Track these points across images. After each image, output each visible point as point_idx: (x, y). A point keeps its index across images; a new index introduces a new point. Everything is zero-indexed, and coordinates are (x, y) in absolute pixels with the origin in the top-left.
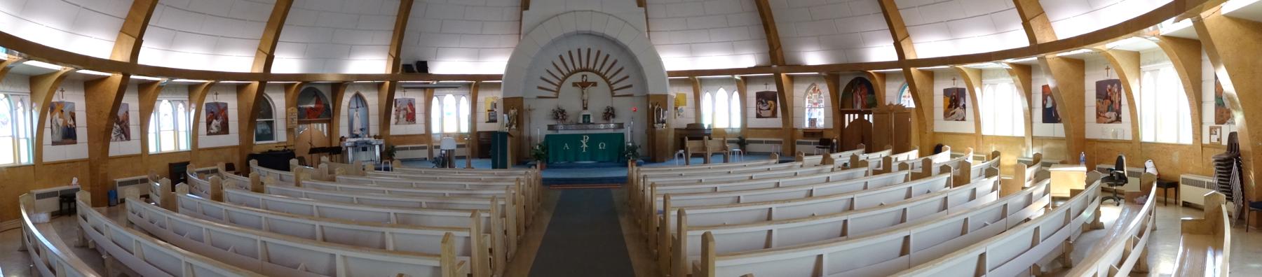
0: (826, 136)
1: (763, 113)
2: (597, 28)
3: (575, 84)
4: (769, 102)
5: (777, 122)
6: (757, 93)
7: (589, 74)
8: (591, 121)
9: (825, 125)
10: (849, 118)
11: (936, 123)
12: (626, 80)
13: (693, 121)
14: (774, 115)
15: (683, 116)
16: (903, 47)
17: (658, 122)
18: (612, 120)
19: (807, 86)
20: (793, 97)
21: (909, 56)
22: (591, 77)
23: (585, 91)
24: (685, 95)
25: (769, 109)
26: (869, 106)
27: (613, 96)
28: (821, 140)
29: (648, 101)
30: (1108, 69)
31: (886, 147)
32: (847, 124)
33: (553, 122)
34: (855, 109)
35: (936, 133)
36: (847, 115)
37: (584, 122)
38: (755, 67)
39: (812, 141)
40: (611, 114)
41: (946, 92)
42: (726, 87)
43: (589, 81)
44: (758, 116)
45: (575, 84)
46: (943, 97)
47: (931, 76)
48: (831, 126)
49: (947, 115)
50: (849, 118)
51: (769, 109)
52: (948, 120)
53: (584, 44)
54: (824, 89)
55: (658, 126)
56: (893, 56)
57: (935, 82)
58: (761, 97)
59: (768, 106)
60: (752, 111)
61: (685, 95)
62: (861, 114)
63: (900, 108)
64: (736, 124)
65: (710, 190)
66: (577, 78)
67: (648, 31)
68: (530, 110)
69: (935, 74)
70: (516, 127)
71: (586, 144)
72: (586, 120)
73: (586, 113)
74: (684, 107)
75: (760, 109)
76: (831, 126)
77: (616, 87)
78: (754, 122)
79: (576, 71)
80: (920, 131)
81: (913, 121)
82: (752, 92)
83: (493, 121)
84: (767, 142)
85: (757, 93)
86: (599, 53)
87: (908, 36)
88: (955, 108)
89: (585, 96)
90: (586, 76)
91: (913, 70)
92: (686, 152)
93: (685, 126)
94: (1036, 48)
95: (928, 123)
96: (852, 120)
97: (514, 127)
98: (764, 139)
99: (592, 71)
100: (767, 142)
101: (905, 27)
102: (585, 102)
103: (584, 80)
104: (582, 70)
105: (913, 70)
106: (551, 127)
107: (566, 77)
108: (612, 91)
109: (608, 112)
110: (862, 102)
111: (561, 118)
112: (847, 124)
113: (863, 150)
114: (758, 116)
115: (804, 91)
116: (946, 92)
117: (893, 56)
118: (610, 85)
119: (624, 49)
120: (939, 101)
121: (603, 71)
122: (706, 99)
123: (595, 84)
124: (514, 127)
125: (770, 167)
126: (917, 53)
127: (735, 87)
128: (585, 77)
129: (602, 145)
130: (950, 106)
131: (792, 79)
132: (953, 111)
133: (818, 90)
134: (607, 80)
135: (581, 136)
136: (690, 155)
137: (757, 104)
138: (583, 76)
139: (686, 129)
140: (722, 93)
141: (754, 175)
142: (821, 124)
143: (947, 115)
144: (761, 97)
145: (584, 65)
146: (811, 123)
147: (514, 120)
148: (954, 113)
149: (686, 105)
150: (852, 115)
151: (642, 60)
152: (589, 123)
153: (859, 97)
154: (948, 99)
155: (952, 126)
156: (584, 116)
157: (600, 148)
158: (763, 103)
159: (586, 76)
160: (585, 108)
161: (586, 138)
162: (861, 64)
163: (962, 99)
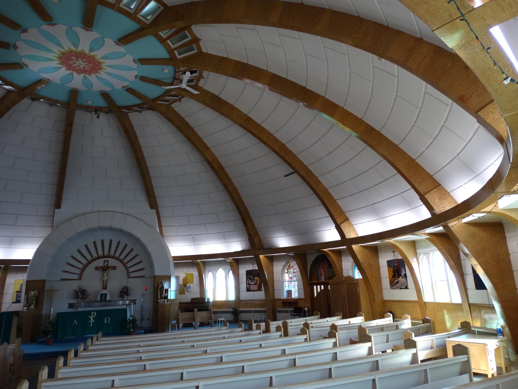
0: (300, 305)
1: (252, 287)
2: (116, 225)
3: (97, 268)
4: (256, 278)
5: (260, 295)
6: (247, 271)
7: (109, 259)
8: (108, 299)
9: (298, 296)
10: (317, 289)
11: (384, 291)
12: (140, 264)
13: (198, 296)
14: (259, 289)
15: (190, 292)
16: (343, 229)
17: (161, 298)
18: (126, 298)
19: (283, 263)
20: (273, 273)
21: (350, 235)
22: (112, 262)
23: (105, 274)
24: (193, 274)
25: (256, 284)
26: (330, 278)
27: (129, 277)
28: (295, 309)
29: (154, 281)
30: (394, 252)
31: (336, 314)
32: (315, 294)
33: (73, 301)
34: (320, 281)
35: (385, 301)
36: (315, 287)
37: (101, 300)
38: (241, 251)
39: (289, 309)
40: (125, 292)
41: (389, 263)
42: (224, 267)
43: (110, 265)
44: (248, 290)
45: (97, 268)
46: (387, 268)
47: (375, 250)
48: (303, 297)
49: (393, 284)
50: (317, 289)
51: (256, 284)
52: (394, 289)
53: (107, 237)
54: (295, 267)
55: (160, 301)
56: (337, 237)
57: (380, 255)
58: (249, 273)
59: (255, 282)
60: (243, 286)
61: (193, 274)
62: (326, 285)
63: (351, 279)
64: (232, 297)
65: (213, 361)
66: (100, 263)
67: (160, 226)
68: (52, 291)
69: (379, 249)
70: (35, 306)
71: (93, 319)
72: (103, 298)
73: (104, 292)
74: (192, 285)
75: (249, 284)
76: (303, 297)
77: (131, 270)
78: (246, 296)
79: (99, 258)
80: (370, 300)
81: (362, 291)
82: (243, 270)
83: (18, 301)
84: (255, 312)
85: (247, 271)
86: (119, 243)
87: (347, 219)
88: (398, 277)
89: (105, 278)
90: (107, 261)
91: (354, 246)
92: (178, 323)
93: (190, 301)
94: (344, 240)
95: (375, 292)
96: (319, 290)
97: (32, 307)
98: (253, 309)
99: (113, 257)
100: (255, 312)
101: (344, 213)
102: (105, 283)
103: (105, 265)
104: (104, 257)
105: (354, 246)
106: (71, 306)
107: (89, 263)
108: (128, 273)
109: (123, 291)
110: (325, 275)
111: (80, 297)
112: (315, 294)
113: (340, 317)
114: (248, 290)
115: (281, 268)
116: (389, 263)
117: (337, 237)
118: (127, 268)
119: (137, 240)
120: (385, 272)
121: (122, 257)
122: (209, 279)
123: (114, 268)
124: (32, 307)
125: (226, 336)
126: (357, 232)
127: (229, 267)
128: (106, 263)
129: (107, 320)
130: (394, 276)
131: (271, 260)
132: (397, 280)
133: (292, 267)
134: (125, 265)
135: (89, 313)
136: (181, 325)
137: (247, 280)
138: (105, 261)
139: (190, 303)
140: (221, 272)
141: (196, 344)
142: (295, 295)
143: (393, 284)
144: (249, 273)
145: (106, 252)
146: (288, 294)
147: (33, 300)
148: (398, 282)
149: (193, 283)
150: (319, 287)
151: (151, 249)
152: (105, 300)
153: (322, 271)
154: (392, 269)
155: (397, 295)
156: (102, 295)
157: (106, 322)
158: (251, 279)
159: (107, 261)
160: (105, 288)
161: (94, 314)
162: (315, 244)
163: (403, 269)
